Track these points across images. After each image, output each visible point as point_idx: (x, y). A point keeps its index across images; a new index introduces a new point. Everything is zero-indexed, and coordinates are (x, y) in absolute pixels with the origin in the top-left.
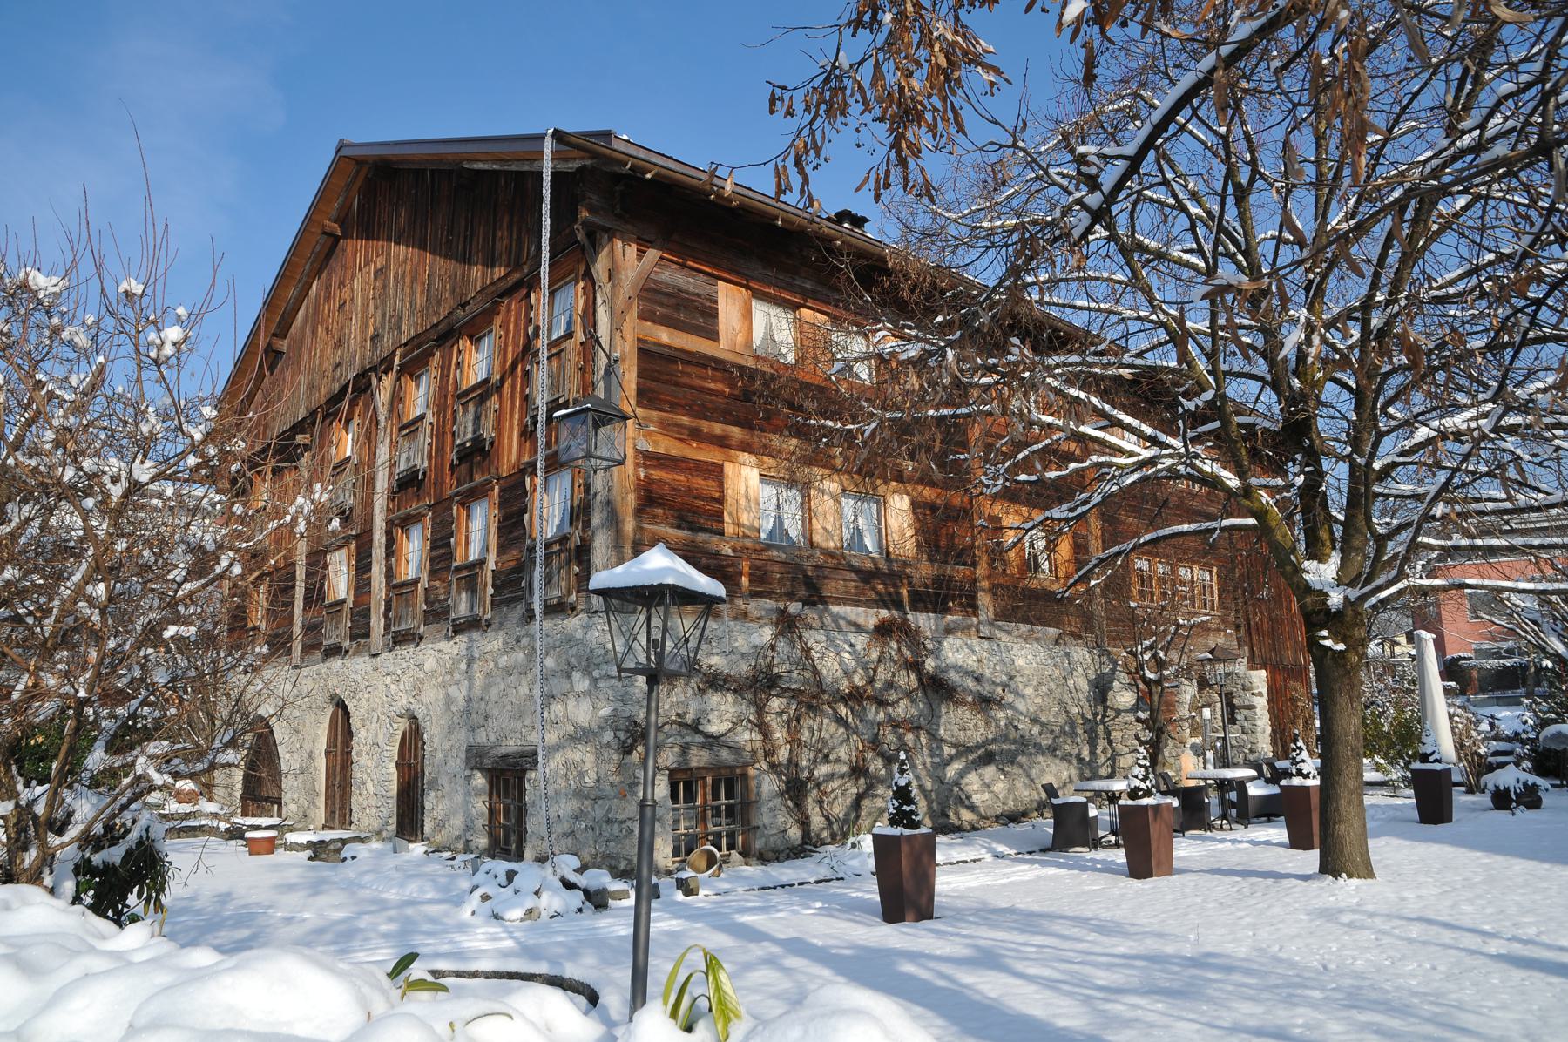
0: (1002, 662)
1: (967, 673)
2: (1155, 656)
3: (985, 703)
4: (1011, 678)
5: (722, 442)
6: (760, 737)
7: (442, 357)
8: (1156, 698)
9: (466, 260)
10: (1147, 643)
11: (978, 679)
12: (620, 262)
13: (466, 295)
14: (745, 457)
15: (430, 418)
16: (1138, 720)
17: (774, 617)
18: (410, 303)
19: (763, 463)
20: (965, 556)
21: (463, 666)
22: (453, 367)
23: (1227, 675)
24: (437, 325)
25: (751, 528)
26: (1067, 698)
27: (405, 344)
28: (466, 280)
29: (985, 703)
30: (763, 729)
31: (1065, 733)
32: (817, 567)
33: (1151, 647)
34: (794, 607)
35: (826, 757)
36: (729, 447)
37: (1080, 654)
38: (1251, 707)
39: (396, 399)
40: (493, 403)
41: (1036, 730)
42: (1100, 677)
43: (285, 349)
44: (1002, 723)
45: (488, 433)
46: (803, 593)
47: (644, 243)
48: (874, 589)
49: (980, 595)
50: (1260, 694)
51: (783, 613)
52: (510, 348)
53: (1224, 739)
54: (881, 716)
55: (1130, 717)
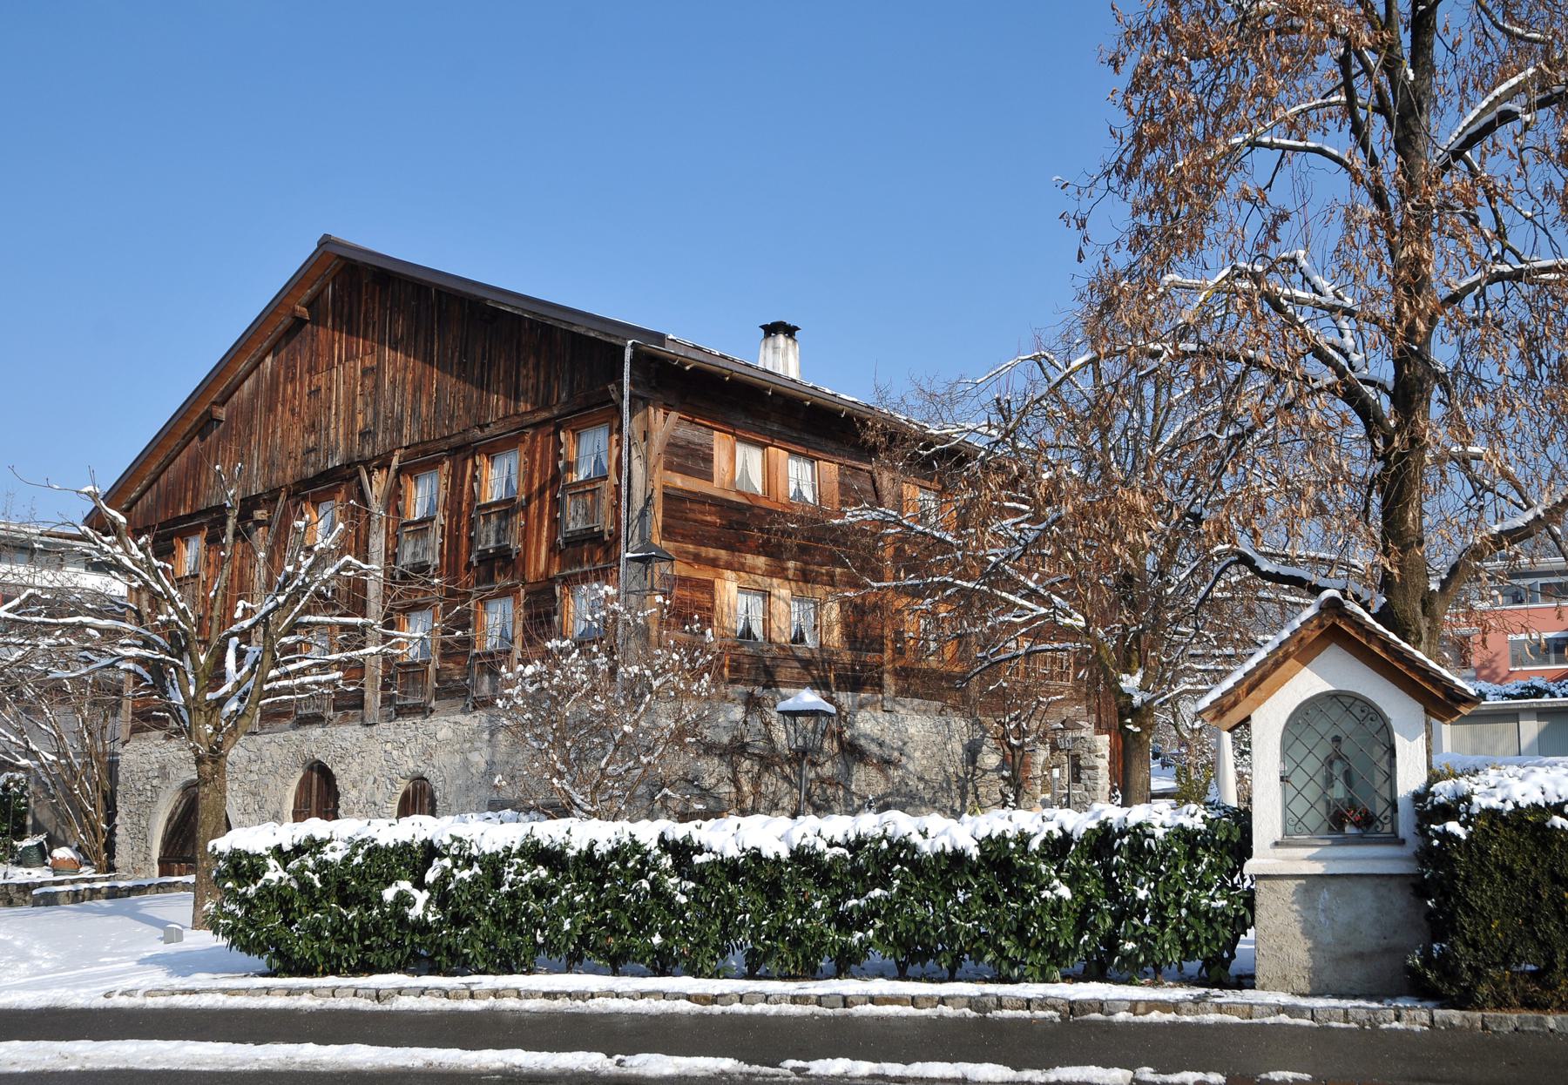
0: (898, 730)
1: (873, 740)
2: (1018, 726)
3: (885, 763)
4: (905, 744)
5: (714, 563)
6: (734, 790)
7: (454, 467)
8: (1017, 760)
9: (484, 385)
10: (1013, 715)
11: (881, 745)
12: (653, 425)
13: (486, 418)
14: (729, 574)
15: (440, 519)
16: (1003, 778)
17: (743, 697)
18: (413, 410)
19: (740, 577)
20: (877, 644)
21: (486, 736)
22: (468, 478)
23: (1075, 740)
24: (449, 437)
25: (731, 629)
26: (945, 760)
27: (406, 448)
28: (483, 405)
29: (885, 763)
30: (735, 782)
31: (942, 788)
32: (774, 658)
33: (1016, 718)
34: (758, 691)
35: (777, 805)
36: (718, 566)
37: (959, 723)
38: (1094, 768)
39: (394, 498)
40: (519, 520)
41: (921, 786)
42: (972, 742)
43: (223, 417)
44: (897, 780)
45: (515, 544)
46: (763, 679)
47: (668, 408)
48: (811, 674)
49: (886, 676)
50: (1103, 756)
51: (751, 695)
52: (537, 475)
53: (1068, 795)
54: (812, 775)
55: (995, 776)
